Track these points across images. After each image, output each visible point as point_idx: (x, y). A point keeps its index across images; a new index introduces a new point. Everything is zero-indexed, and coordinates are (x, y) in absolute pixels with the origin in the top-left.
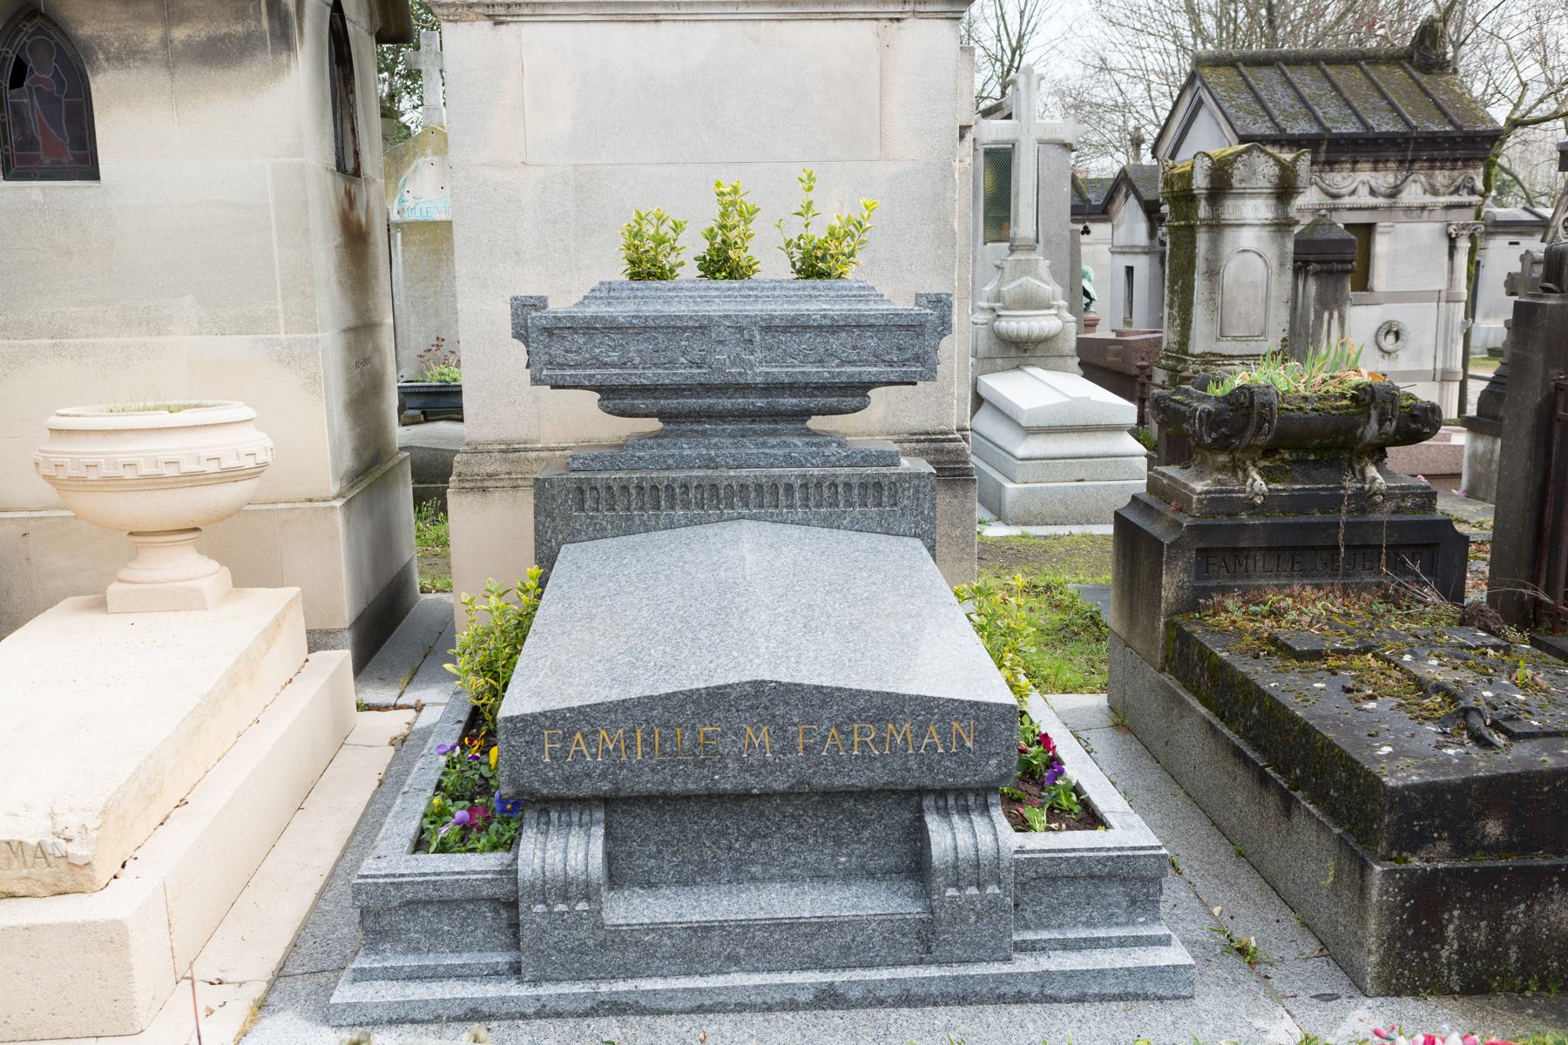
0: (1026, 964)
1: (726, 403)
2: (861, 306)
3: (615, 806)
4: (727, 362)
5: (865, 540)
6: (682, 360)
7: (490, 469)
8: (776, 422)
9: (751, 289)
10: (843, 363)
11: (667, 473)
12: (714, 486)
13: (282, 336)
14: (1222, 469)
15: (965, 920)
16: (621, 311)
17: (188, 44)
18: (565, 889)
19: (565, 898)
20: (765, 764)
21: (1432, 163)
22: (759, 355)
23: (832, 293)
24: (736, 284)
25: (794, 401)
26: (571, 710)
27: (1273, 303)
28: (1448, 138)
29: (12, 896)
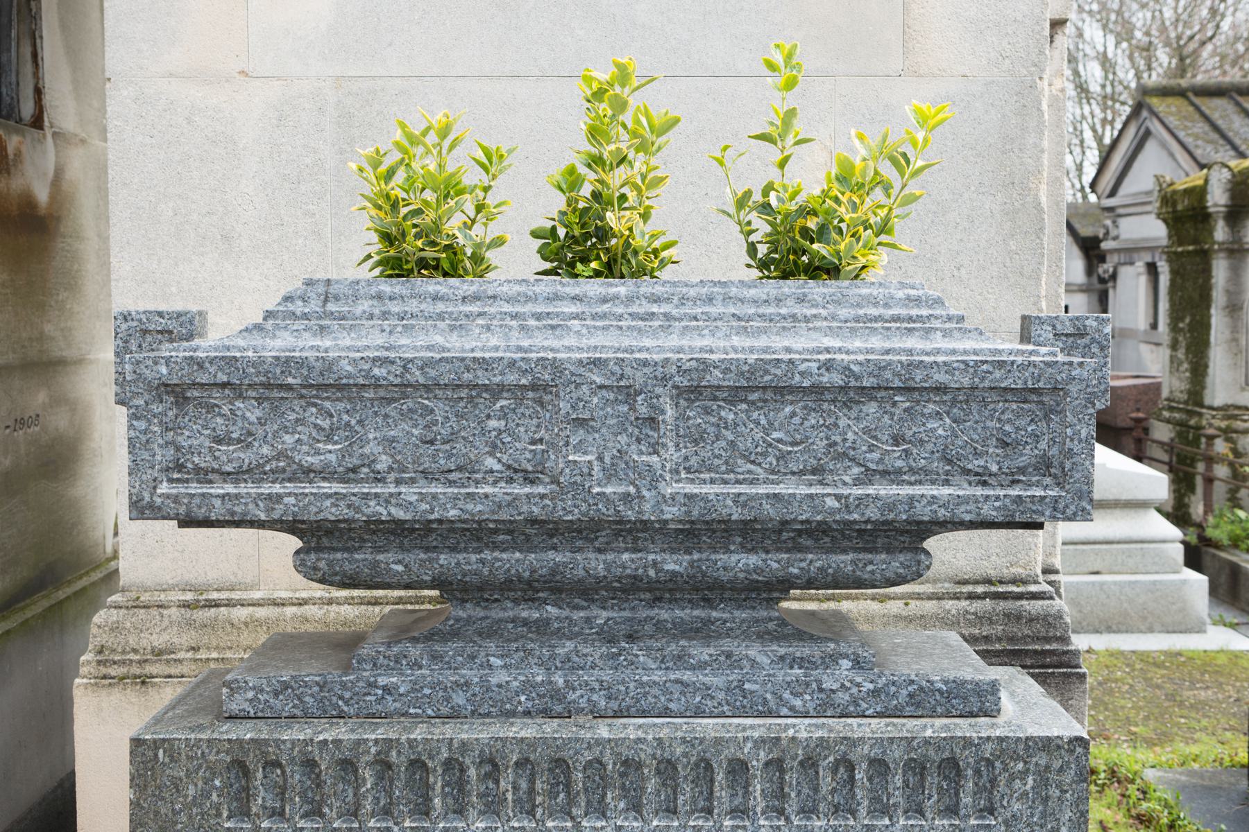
1: (593, 563)
2: (912, 342)
4: (591, 467)
6: (491, 463)
7: (159, 641)
8: (708, 603)
9: (656, 300)
11: (448, 731)
12: (560, 762)
16: (347, 346)
22: (672, 454)
23: (844, 312)
24: (621, 288)
25: (753, 560)
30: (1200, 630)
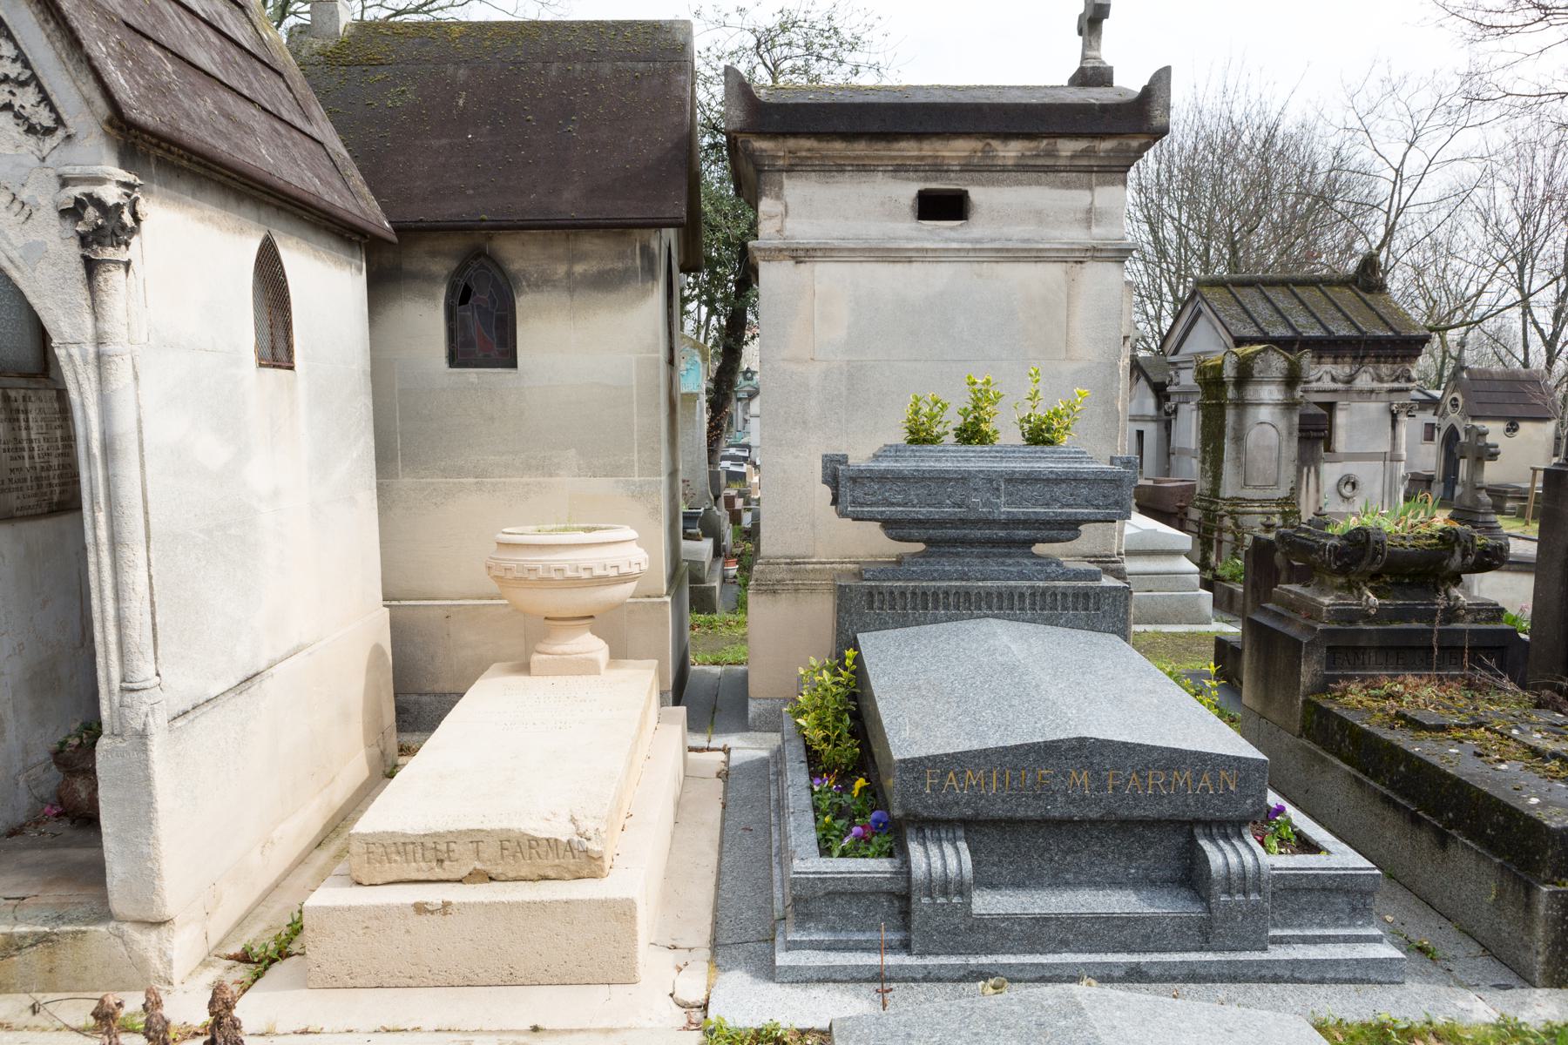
0: (1278, 953)
3: (973, 827)
4: (979, 503)
5: (1081, 635)
7: (779, 577)
10: (1063, 506)
13: (636, 479)
14: (1340, 588)
15: (1234, 919)
16: (906, 465)
17: (584, 275)
18: (945, 886)
19: (945, 893)
20: (1084, 798)
21: (1378, 359)
26: (947, 755)
27: (1283, 462)
28: (1389, 340)
29: (546, 878)
30: (1208, 623)
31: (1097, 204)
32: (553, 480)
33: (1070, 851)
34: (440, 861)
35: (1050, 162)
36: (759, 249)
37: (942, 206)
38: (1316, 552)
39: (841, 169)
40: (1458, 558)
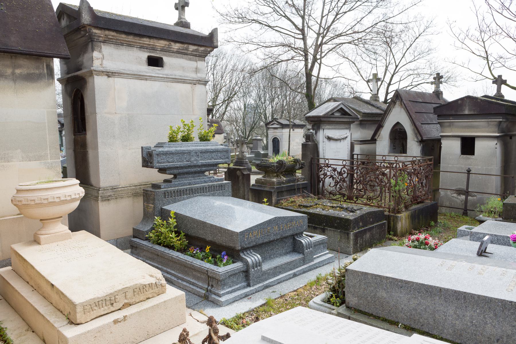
0: (316, 261)
3: (257, 247)
7: (109, 194)
13: (49, 161)
19: (257, 267)
20: (277, 233)
31: (198, 66)
32: (10, 163)
33: (272, 249)
34: (112, 304)
35: (186, 52)
36: (95, 71)
37: (154, 62)
38: (271, 167)
39: (122, 45)
40: (298, 166)
